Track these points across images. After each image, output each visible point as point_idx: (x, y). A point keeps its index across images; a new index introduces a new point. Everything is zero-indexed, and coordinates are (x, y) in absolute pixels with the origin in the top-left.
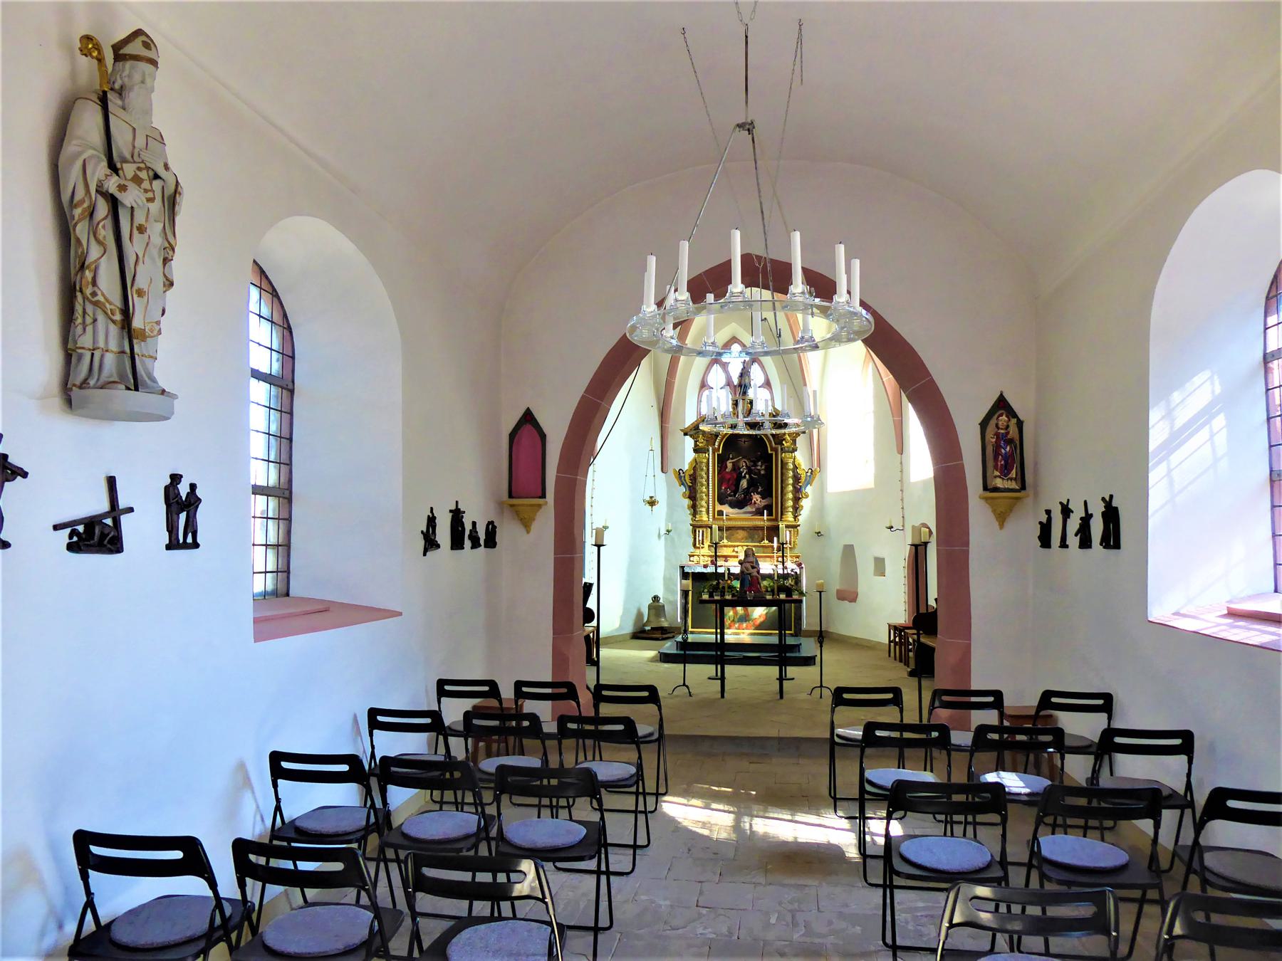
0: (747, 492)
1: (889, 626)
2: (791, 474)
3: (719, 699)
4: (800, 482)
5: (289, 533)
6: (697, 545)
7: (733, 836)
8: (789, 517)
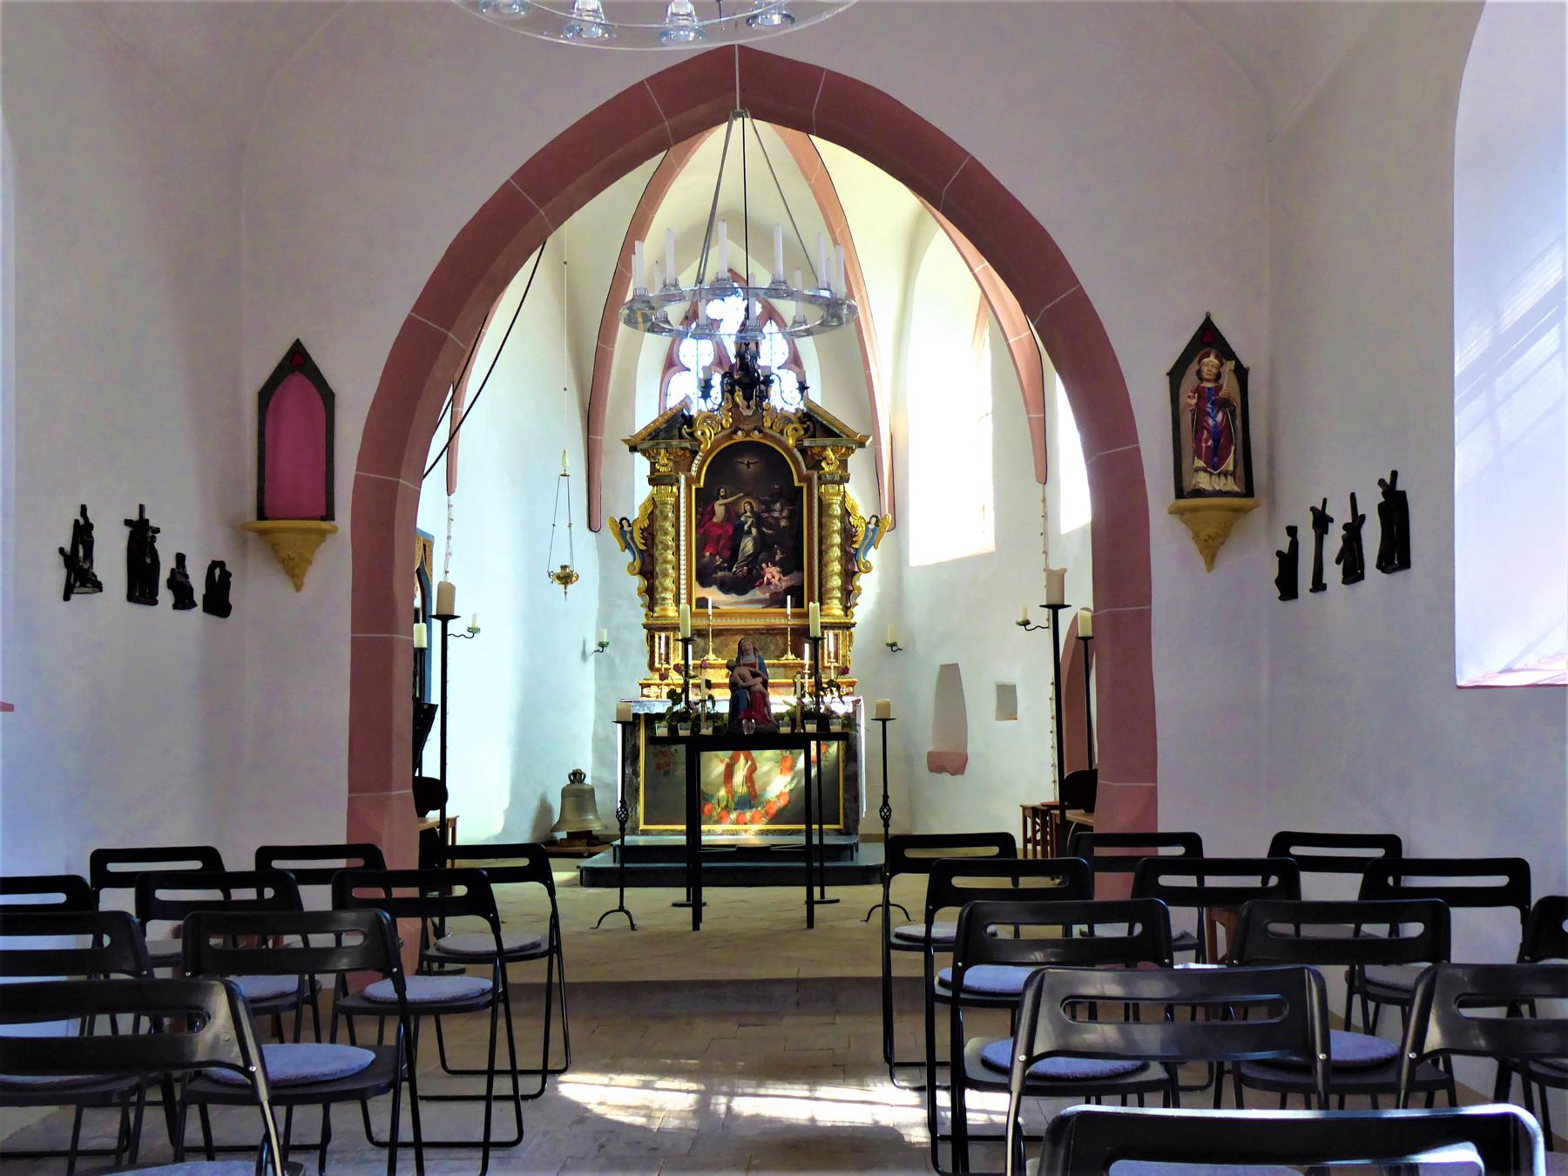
0: (753, 560)
1: (1024, 808)
2: (837, 525)
3: (689, 932)
4: (855, 542)
6: (657, 665)
7: (693, 1124)
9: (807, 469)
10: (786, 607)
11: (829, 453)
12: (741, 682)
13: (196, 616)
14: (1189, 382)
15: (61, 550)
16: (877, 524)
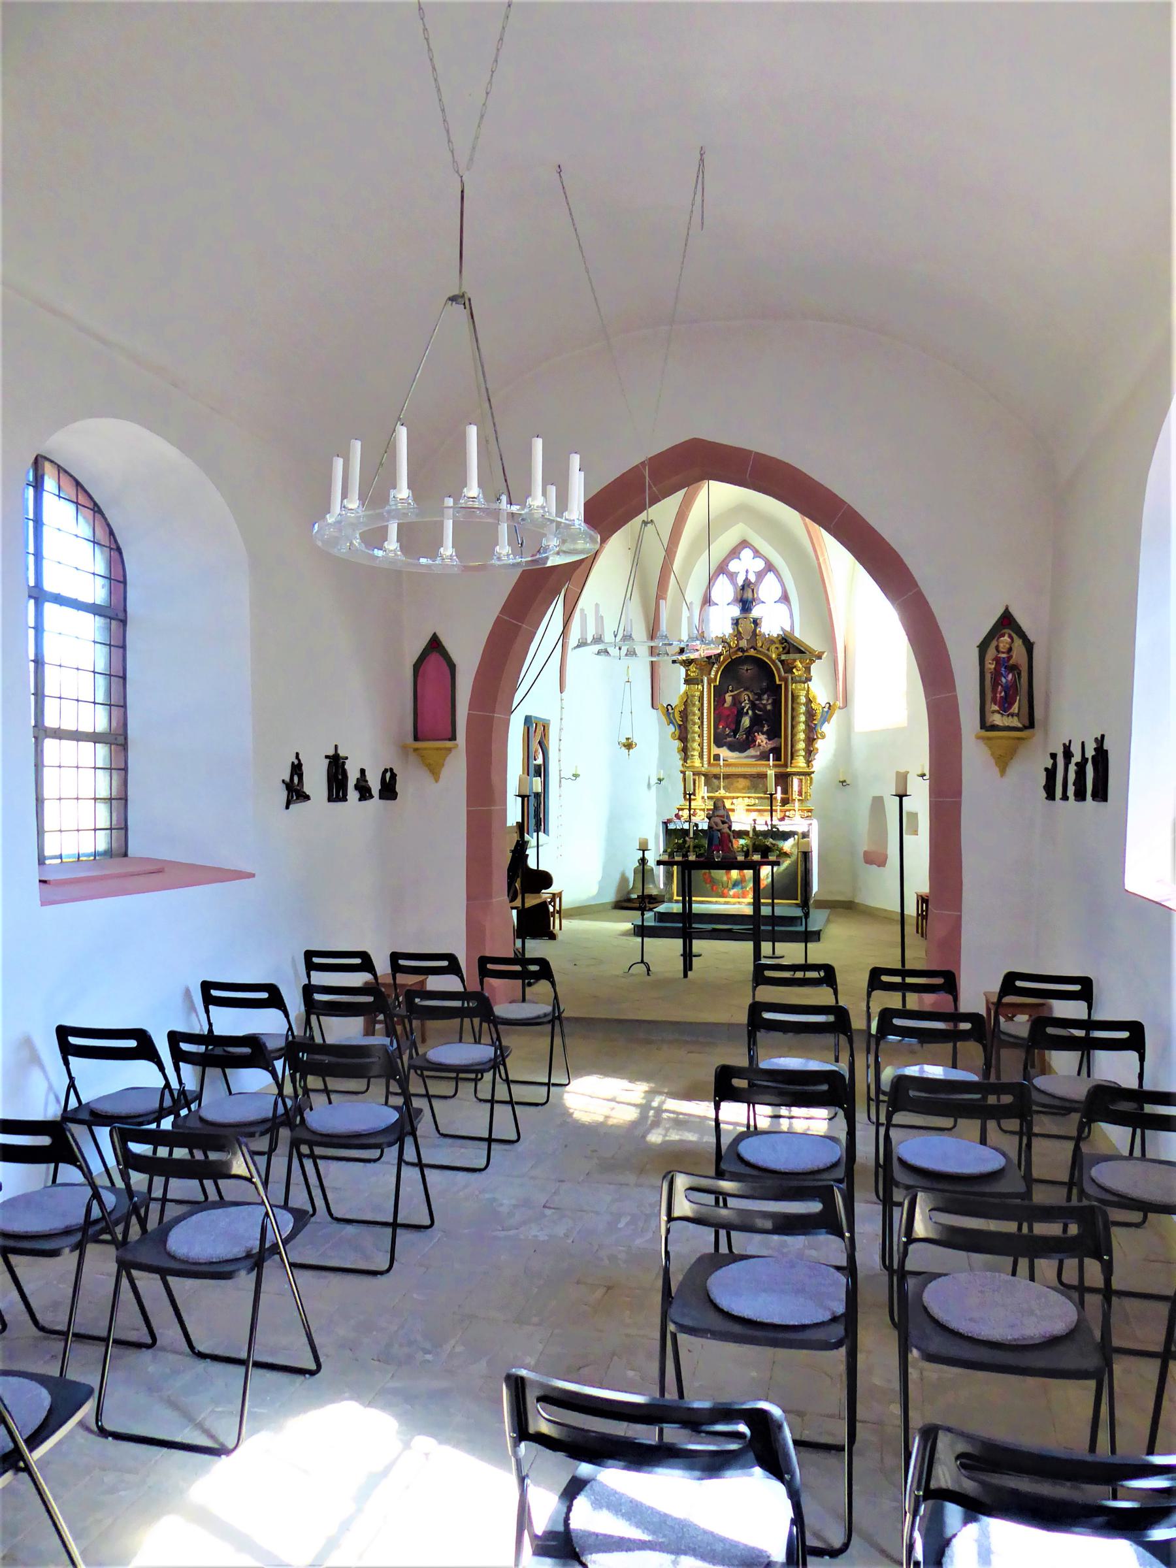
0: (750, 732)
2: (803, 709)
5: (125, 783)
8: (800, 763)
9: (785, 673)
10: (769, 760)
11: (798, 663)
12: (715, 826)
13: (375, 802)
14: (991, 653)
15: (283, 781)
16: (829, 708)
